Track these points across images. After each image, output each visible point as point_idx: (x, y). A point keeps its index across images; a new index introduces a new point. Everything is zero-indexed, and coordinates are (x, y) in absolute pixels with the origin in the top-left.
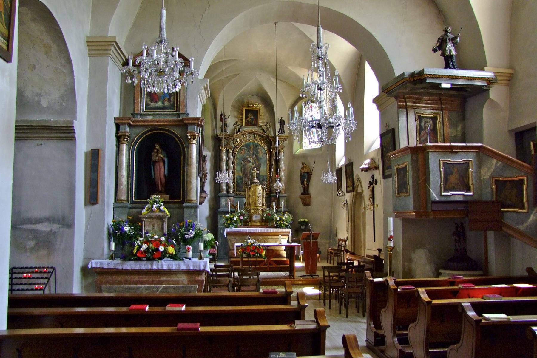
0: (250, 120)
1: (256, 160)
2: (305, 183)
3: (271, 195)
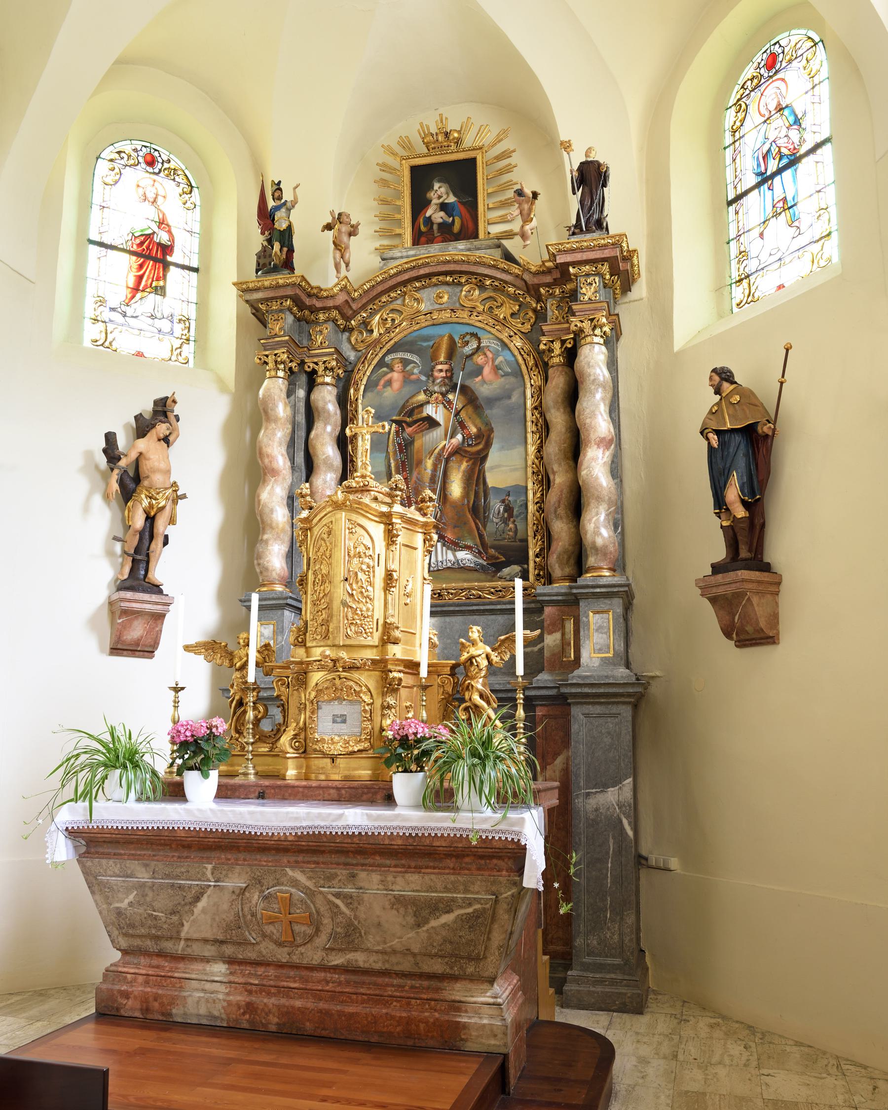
0: (439, 217)
1: (463, 414)
2: (733, 493)
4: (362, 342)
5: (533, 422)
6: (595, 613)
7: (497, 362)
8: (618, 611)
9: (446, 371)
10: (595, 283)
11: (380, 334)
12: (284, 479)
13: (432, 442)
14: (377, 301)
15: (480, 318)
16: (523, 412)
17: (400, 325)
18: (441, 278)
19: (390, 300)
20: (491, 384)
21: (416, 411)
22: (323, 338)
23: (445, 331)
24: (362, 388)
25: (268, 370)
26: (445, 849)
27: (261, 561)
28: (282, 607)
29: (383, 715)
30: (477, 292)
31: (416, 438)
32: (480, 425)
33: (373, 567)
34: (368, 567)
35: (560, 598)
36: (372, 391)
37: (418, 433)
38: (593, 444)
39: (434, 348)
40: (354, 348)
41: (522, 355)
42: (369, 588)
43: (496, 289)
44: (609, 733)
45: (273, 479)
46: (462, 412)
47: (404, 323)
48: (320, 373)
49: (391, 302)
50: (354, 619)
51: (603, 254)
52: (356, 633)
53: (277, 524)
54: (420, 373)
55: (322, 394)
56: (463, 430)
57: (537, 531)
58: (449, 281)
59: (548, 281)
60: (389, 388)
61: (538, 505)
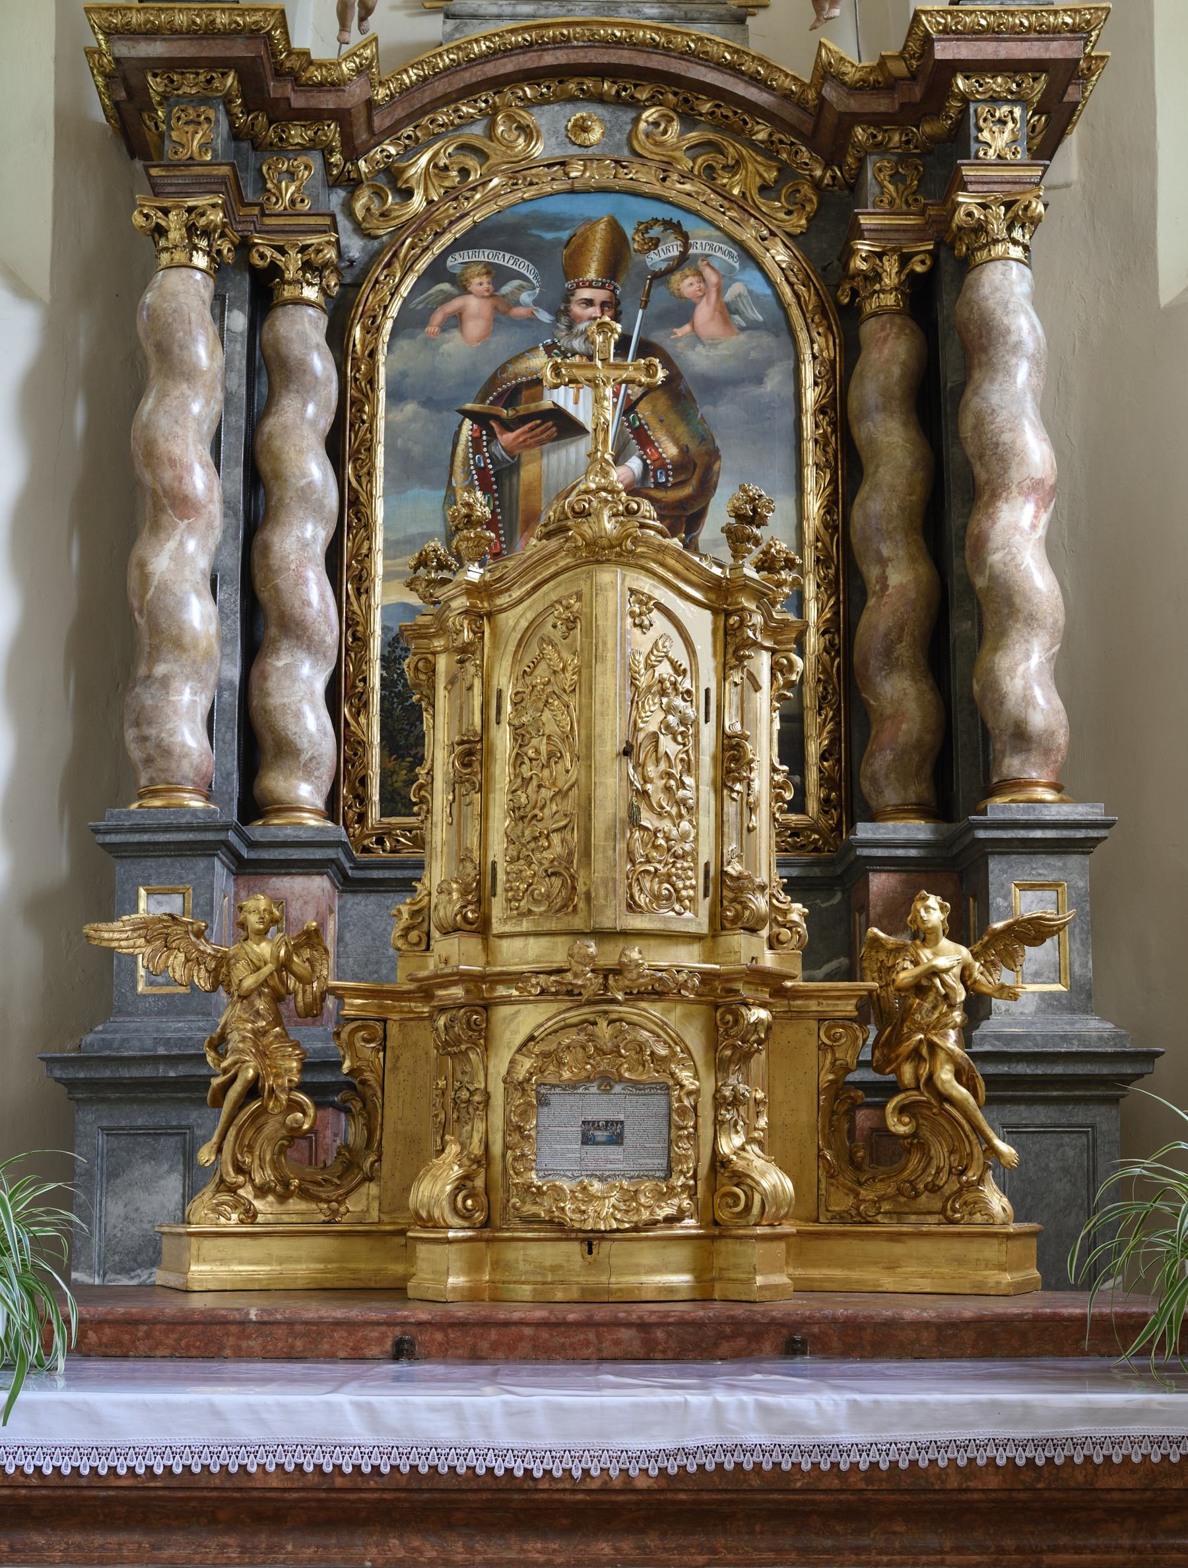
1: (644, 411)
3: (864, 831)
4: (382, 215)
5: (816, 441)
6: (1024, 888)
7: (729, 296)
8: (1081, 884)
9: (603, 304)
10: (1014, 120)
11: (430, 202)
12: (210, 526)
13: (566, 472)
14: (425, 121)
15: (687, 187)
16: (790, 417)
17: (485, 184)
18: (589, 84)
19: (457, 121)
20: (714, 346)
21: (525, 394)
22: (298, 190)
23: (599, 208)
24: (389, 325)
25: (166, 249)
26: (1128, 1496)
27: (152, 732)
28: (205, 850)
29: (718, 1123)
30: (676, 126)
31: (524, 459)
32: (685, 440)
33: (695, 722)
34: (683, 722)
35: (913, 853)
36: (412, 337)
37: (530, 446)
38: (1015, 494)
39: (572, 246)
40: (360, 229)
41: (791, 285)
42: (689, 780)
43: (720, 124)
44: (1066, 1170)
45: (182, 525)
46: (642, 404)
47: (496, 181)
48: (289, 275)
49: (460, 126)
50: (648, 861)
51: (1047, 49)
52: (656, 897)
53: (195, 638)
54: (536, 303)
55: (298, 327)
56: (643, 448)
57: (824, 698)
58: (608, 93)
59: (882, 109)
60: (455, 333)
61: (827, 636)
